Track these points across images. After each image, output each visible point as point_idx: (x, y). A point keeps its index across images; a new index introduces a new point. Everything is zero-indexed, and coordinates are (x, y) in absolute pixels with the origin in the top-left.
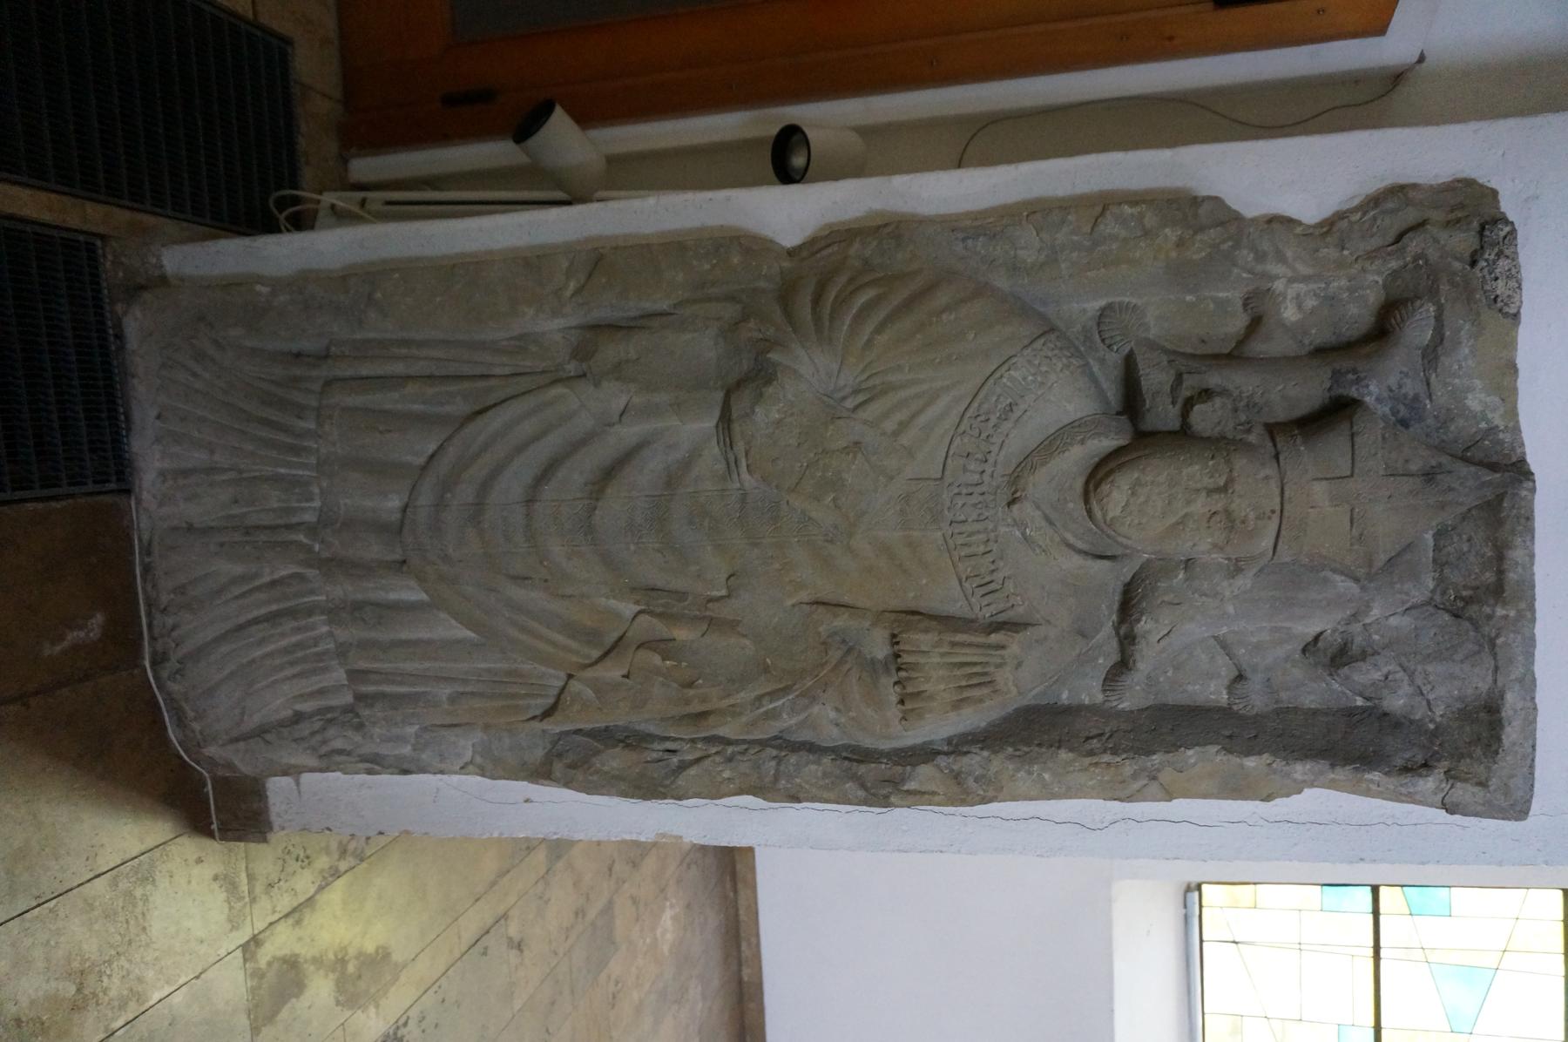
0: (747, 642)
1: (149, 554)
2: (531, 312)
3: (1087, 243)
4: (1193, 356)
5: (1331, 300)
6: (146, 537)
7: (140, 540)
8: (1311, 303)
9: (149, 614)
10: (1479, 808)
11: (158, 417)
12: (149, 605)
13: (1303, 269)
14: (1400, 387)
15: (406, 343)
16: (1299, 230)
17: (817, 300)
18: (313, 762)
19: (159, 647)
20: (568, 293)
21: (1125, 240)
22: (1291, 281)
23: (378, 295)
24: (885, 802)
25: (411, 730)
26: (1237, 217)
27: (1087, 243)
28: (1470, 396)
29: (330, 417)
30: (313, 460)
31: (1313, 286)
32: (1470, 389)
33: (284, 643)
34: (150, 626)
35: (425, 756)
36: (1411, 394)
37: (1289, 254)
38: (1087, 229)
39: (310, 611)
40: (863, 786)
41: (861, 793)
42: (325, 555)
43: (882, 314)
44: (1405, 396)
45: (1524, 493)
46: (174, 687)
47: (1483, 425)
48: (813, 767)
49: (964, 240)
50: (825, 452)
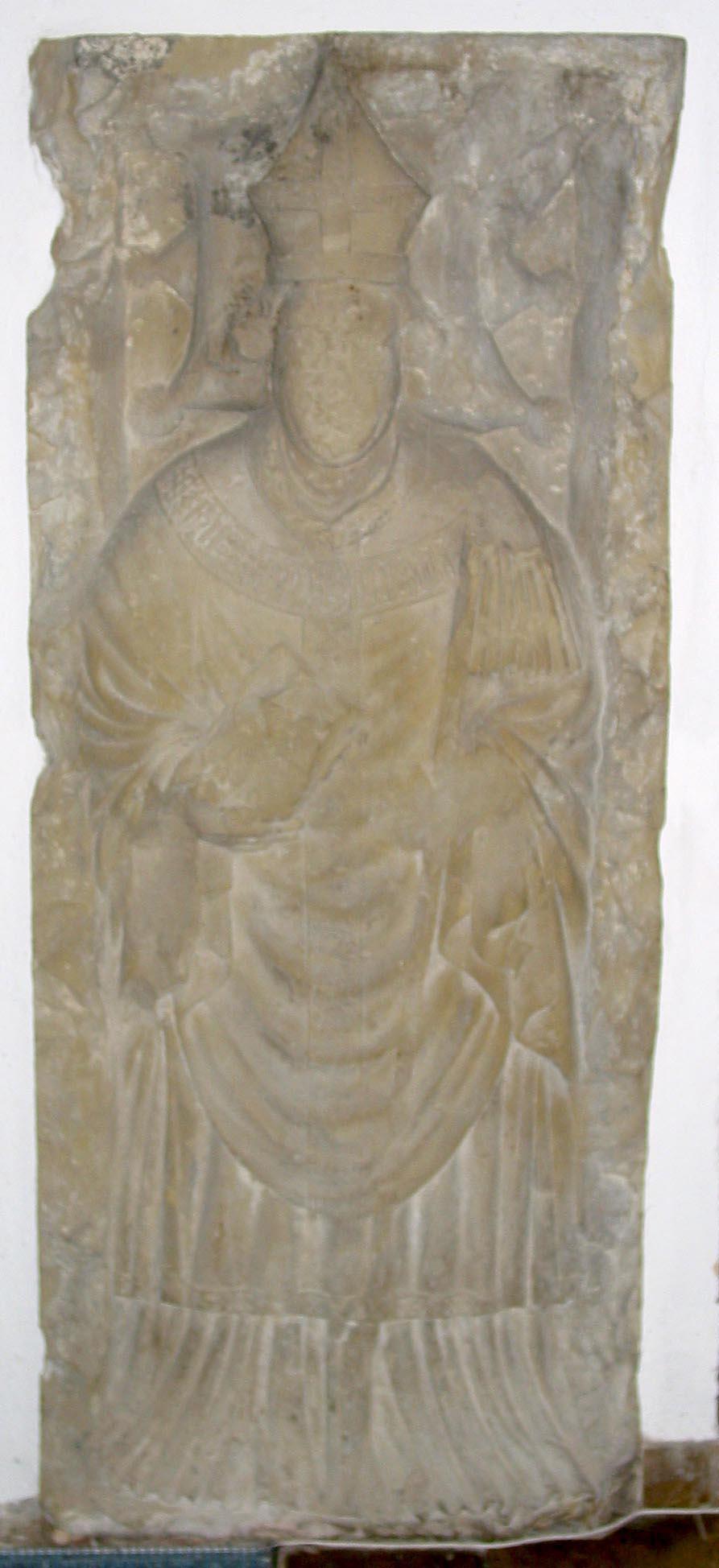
0: (476, 833)
1: (350, 1529)
2: (96, 1055)
3: (67, 451)
4: (192, 345)
5: (141, 202)
6: (331, 1531)
7: (335, 1538)
8: (143, 222)
9: (425, 1538)
10: (674, 85)
11: (191, 1498)
12: (414, 1536)
13: (108, 230)
14: (234, 151)
15: (123, 1209)
16: (68, 232)
17: (107, 733)
18: (625, 1370)
19: (466, 1531)
20: (78, 1008)
21: (66, 413)
22: (119, 243)
23: (65, 1230)
24: (664, 693)
25: (584, 1244)
26: (52, 298)
27: (67, 451)
28: (248, 81)
29: (203, 1293)
30: (252, 1320)
31: (126, 219)
32: (241, 83)
33: (470, 1384)
34: (439, 1538)
35: (621, 1235)
36: (242, 140)
37: (91, 245)
38: (52, 450)
39: (431, 1342)
40: (645, 716)
41: (653, 720)
42: (360, 1312)
43: (128, 669)
44: (244, 145)
45: (346, 44)
46: (516, 1521)
47: (278, 69)
48: (625, 771)
49: (52, 576)
50: (269, 734)
